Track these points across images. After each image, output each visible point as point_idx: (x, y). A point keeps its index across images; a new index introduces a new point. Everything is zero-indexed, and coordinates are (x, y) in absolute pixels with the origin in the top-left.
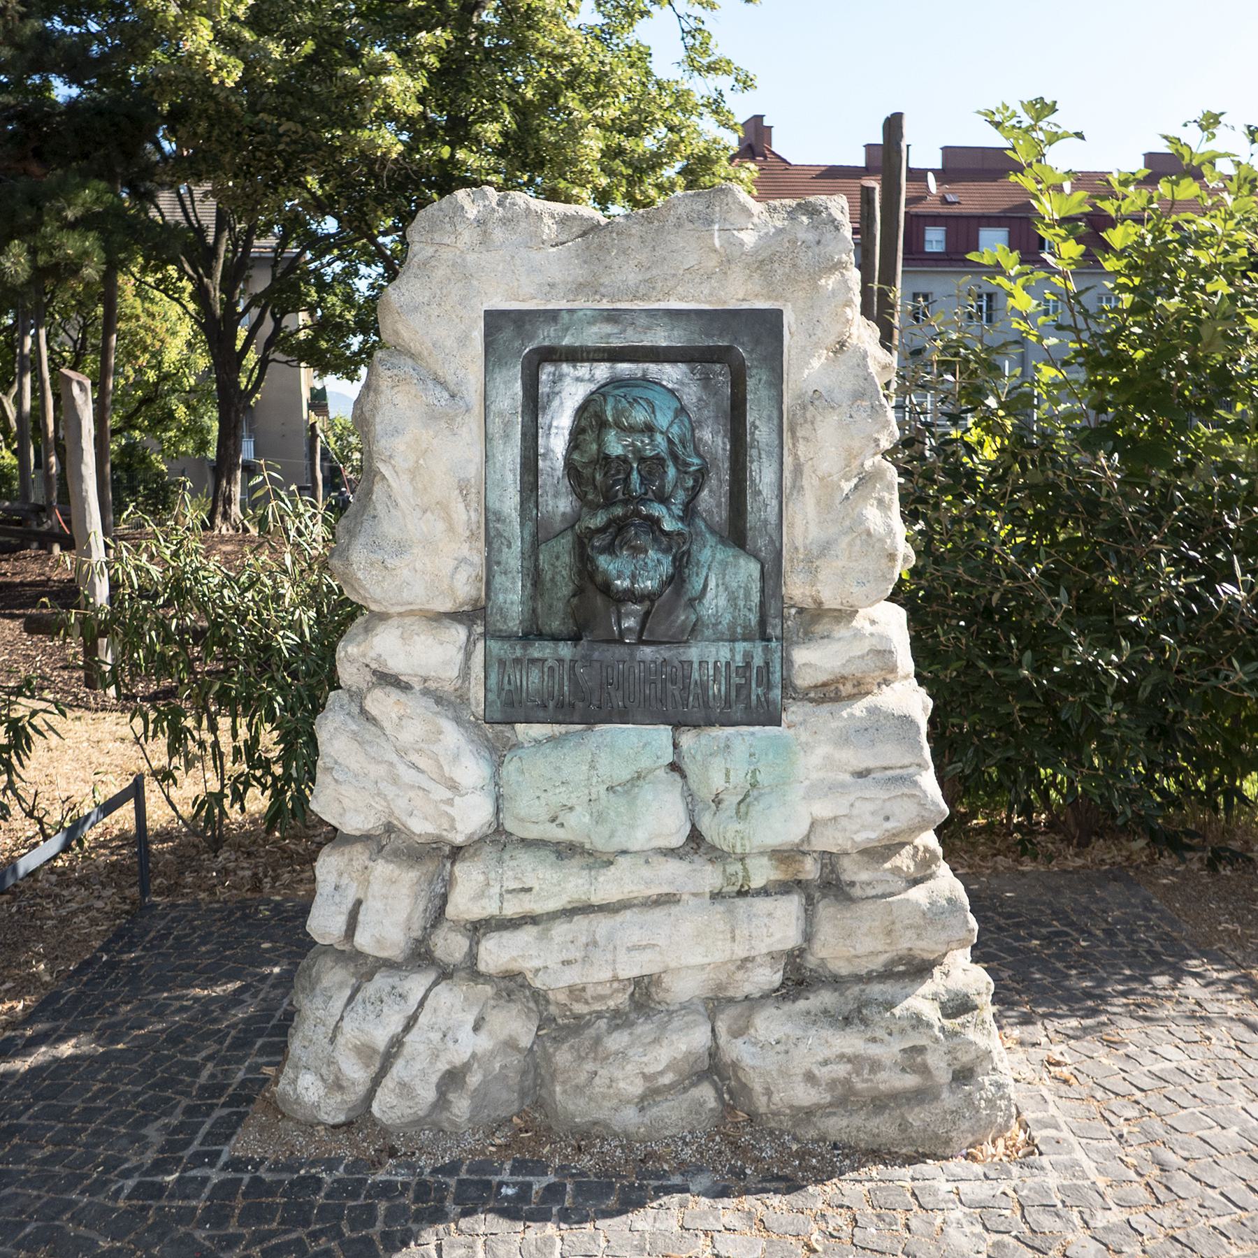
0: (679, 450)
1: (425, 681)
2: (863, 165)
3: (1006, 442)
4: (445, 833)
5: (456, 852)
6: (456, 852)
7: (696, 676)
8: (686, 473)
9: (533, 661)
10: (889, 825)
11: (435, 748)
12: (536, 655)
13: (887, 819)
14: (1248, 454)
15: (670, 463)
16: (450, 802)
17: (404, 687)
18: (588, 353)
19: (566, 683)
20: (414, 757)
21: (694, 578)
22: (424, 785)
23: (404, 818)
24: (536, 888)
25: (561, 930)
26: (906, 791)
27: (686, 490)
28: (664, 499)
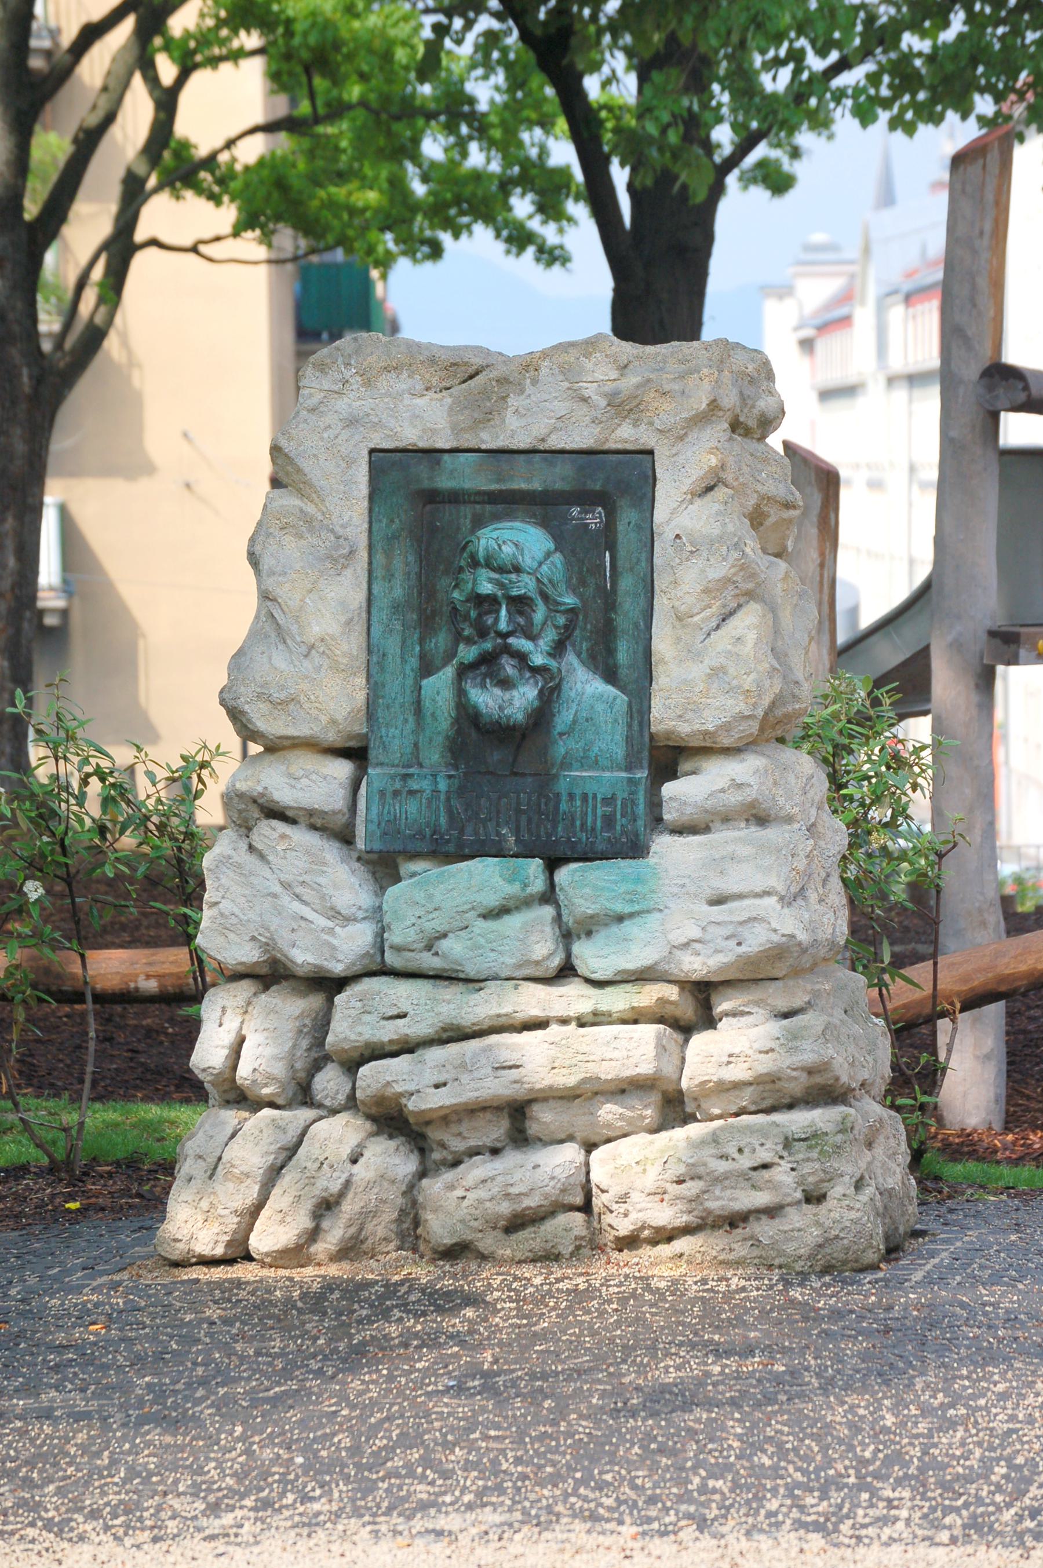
0: (550, 591)
1: (311, 815)
2: (768, 440)
3: (575, 9)
4: (325, 963)
5: (338, 984)
6: (338, 984)
7: (564, 806)
8: (557, 611)
9: (412, 793)
10: (741, 950)
11: (322, 880)
12: (415, 787)
13: (739, 944)
14: (976, 78)
15: (539, 602)
16: (331, 931)
17: (292, 821)
18: (469, 495)
19: (442, 814)
20: (299, 890)
21: (564, 713)
22: (308, 917)
23: (286, 949)
24: (412, 1013)
25: (436, 1054)
26: (393, 662)
27: (556, 627)
28: (532, 638)
